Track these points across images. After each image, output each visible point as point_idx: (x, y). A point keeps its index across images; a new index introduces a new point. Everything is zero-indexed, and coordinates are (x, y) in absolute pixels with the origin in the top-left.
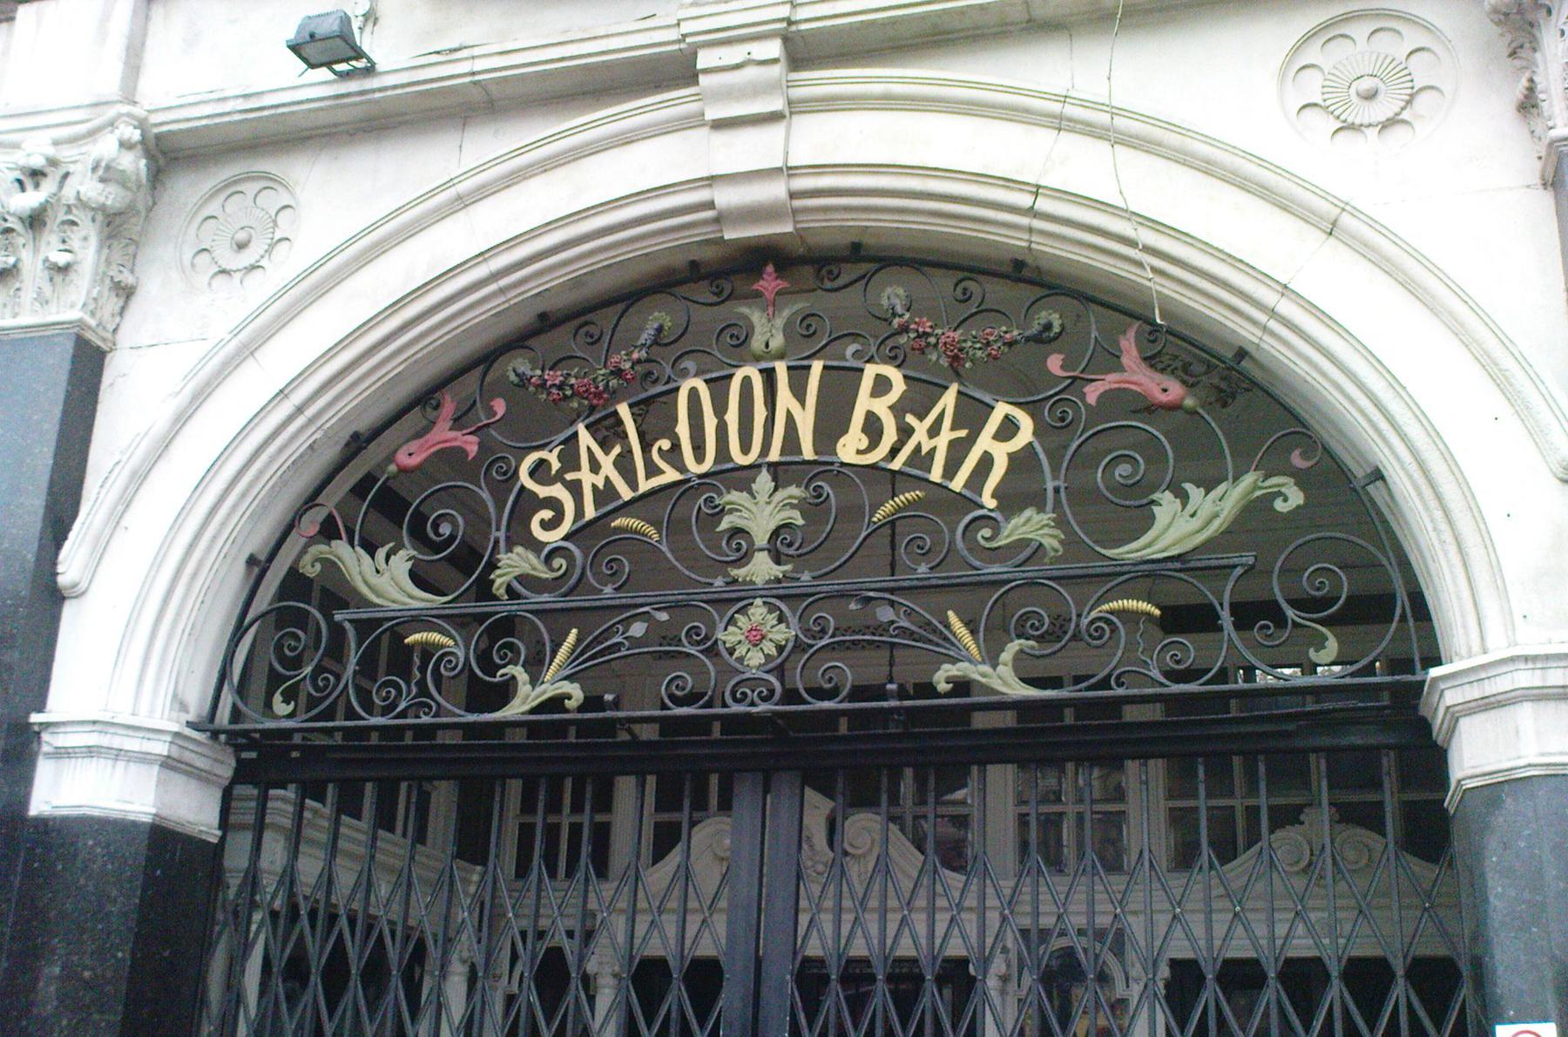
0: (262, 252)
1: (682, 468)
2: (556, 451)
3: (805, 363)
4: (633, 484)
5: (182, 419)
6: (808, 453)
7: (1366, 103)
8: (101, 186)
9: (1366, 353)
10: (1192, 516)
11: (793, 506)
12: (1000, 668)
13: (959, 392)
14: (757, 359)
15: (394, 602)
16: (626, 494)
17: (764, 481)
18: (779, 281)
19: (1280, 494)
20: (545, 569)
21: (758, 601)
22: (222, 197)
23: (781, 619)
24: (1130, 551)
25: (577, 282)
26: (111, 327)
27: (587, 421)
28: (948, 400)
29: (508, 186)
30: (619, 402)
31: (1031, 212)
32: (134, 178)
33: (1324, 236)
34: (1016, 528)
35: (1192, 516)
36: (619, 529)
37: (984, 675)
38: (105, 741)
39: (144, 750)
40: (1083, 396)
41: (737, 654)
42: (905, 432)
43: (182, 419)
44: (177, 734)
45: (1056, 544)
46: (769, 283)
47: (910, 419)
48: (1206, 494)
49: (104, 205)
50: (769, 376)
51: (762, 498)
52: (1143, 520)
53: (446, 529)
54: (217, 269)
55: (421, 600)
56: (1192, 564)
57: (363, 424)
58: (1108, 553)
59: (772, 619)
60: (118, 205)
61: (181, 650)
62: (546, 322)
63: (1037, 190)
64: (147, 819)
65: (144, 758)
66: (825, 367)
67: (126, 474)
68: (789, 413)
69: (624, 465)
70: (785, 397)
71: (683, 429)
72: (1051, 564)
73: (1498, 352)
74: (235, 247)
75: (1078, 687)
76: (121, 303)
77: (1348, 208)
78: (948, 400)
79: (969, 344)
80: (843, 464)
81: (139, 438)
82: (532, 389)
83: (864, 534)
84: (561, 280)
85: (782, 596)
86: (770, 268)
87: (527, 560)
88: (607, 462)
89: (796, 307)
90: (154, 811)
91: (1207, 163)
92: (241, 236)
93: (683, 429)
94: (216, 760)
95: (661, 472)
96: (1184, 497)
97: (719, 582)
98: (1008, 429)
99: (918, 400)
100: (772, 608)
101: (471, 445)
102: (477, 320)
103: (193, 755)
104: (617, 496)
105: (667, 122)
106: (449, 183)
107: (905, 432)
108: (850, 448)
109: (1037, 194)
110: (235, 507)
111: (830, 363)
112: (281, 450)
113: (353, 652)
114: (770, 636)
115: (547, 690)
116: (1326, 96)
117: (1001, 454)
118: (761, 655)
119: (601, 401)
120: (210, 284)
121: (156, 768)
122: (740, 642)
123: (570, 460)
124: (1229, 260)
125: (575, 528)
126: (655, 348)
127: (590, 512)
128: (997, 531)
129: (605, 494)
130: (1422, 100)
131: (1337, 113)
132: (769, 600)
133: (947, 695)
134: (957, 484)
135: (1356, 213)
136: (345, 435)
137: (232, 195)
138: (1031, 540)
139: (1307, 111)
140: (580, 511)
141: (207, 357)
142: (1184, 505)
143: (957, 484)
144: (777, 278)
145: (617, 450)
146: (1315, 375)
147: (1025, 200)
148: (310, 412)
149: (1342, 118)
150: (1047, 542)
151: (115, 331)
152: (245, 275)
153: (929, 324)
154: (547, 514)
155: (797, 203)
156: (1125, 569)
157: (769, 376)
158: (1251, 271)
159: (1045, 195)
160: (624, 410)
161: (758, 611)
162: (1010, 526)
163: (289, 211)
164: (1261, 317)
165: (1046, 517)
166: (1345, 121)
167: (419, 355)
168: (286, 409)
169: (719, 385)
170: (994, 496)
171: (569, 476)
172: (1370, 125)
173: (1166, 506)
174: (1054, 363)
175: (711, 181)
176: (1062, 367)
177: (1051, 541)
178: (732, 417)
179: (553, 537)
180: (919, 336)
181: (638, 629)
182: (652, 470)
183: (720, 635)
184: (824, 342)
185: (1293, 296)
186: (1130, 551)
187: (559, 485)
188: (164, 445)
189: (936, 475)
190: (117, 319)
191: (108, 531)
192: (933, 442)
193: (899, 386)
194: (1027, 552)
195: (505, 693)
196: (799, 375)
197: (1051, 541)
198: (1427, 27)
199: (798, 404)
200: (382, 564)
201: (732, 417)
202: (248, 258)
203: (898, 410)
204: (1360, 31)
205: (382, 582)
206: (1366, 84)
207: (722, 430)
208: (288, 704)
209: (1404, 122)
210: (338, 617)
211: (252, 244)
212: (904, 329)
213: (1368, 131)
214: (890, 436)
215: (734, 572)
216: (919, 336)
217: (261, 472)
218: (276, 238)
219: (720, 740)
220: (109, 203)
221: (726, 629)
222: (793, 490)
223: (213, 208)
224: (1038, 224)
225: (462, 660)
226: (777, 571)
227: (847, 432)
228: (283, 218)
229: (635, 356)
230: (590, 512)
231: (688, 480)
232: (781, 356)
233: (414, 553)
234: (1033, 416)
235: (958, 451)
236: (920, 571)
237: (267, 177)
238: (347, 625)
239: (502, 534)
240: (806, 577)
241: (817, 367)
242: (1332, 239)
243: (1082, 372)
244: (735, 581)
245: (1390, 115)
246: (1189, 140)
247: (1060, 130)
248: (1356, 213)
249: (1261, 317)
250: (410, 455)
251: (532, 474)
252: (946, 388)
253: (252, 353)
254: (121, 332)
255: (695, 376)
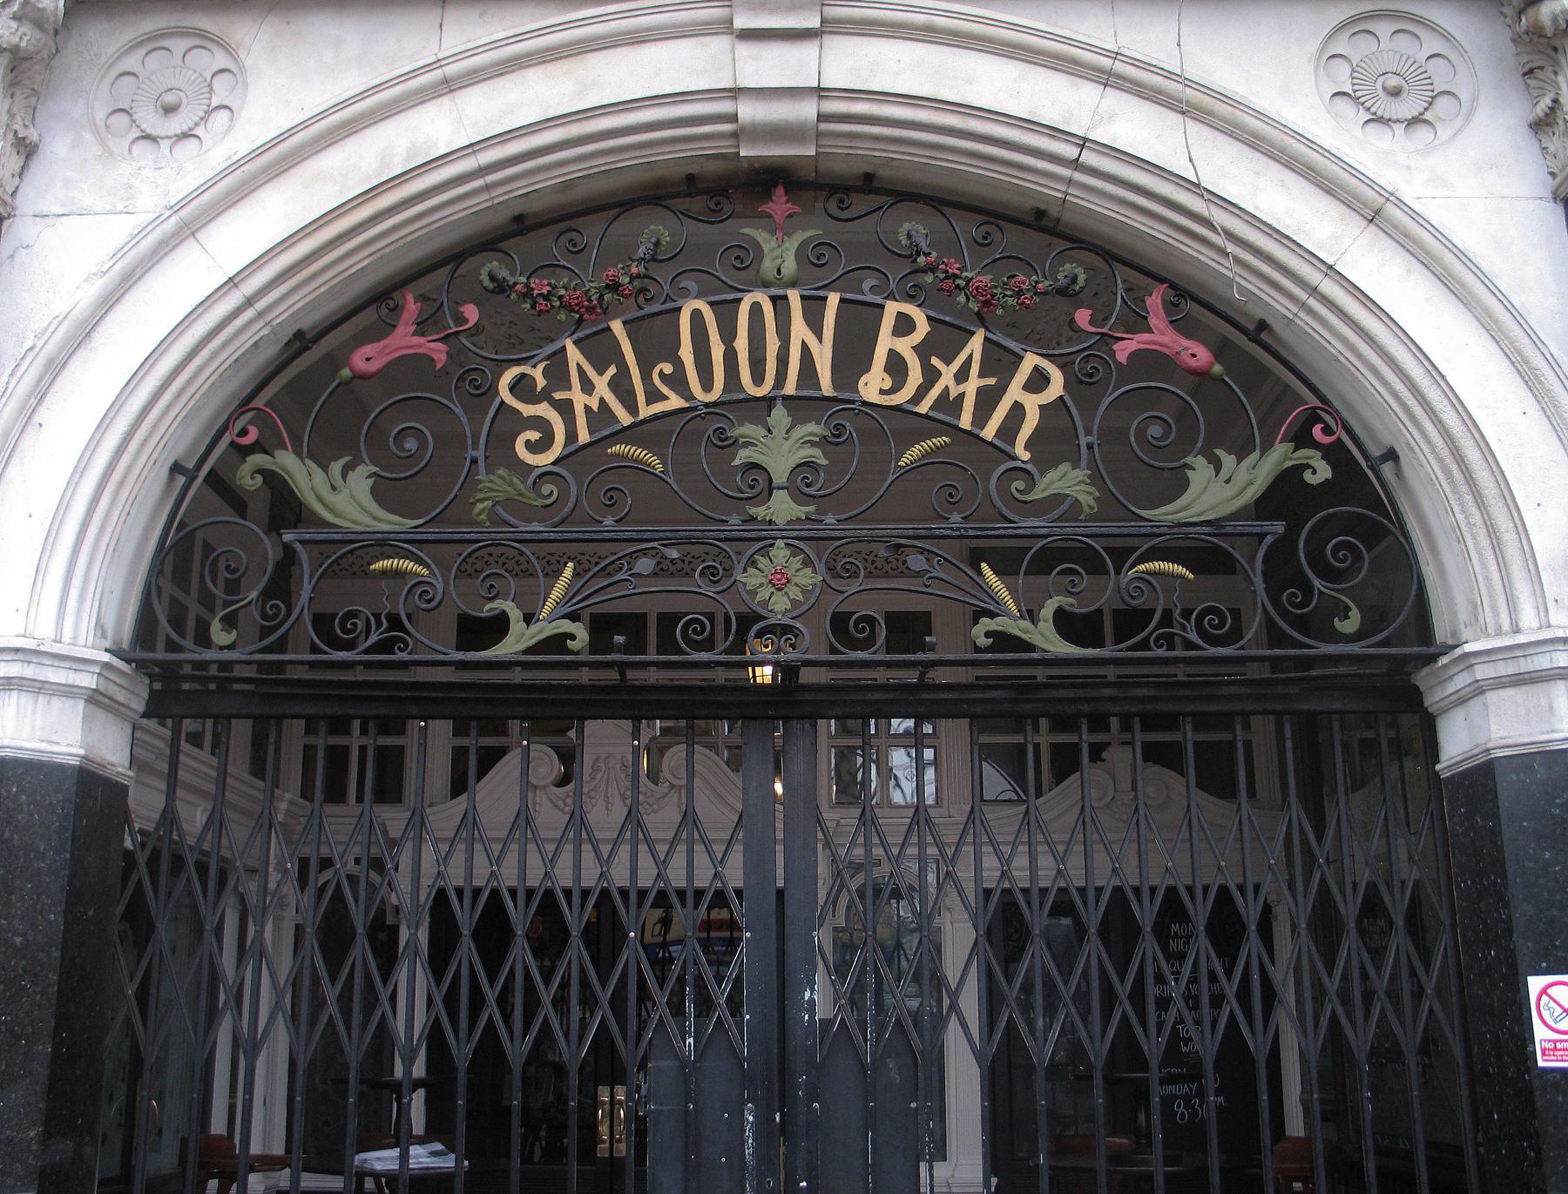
0: (197, 119)
1: (685, 393)
2: (541, 367)
3: (821, 293)
4: (632, 408)
5: (109, 302)
6: (826, 387)
7: (1393, 99)
8: (14, 24)
9: (1406, 340)
10: (1228, 481)
11: (813, 444)
12: (1041, 624)
13: (986, 339)
14: (766, 285)
15: (355, 522)
16: (625, 419)
17: (779, 414)
18: (789, 205)
19: (1308, 466)
20: (533, 495)
21: (780, 543)
22: (142, 52)
23: (808, 562)
24: (1165, 513)
25: (567, 185)
26: (10, 190)
27: (575, 336)
28: (976, 345)
29: (501, 74)
30: (614, 318)
31: (1075, 164)
32: (52, 19)
33: (1365, 223)
34: (1052, 482)
35: (1228, 481)
36: (616, 455)
37: (1026, 632)
38: (29, 671)
39: (70, 682)
40: (1113, 354)
41: (759, 598)
42: (931, 376)
43: (109, 302)
44: (106, 666)
45: (1093, 503)
46: (779, 204)
47: (935, 361)
48: (1239, 461)
49: (17, 47)
50: (779, 302)
51: (779, 432)
52: (1178, 484)
53: (411, 444)
54: (138, 134)
55: (388, 522)
56: (1229, 530)
57: (306, 323)
58: (1144, 513)
59: (796, 562)
60: (31, 48)
61: (104, 569)
62: (521, 224)
63: (1083, 143)
64: (74, 762)
65: (68, 691)
66: (842, 300)
67: (40, 361)
68: (804, 345)
69: (621, 386)
70: (799, 329)
71: (686, 353)
72: (1086, 521)
73: (1530, 352)
74: (161, 110)
75: (1121, 646)
76: (21, 163)
77: (1392, 198)
78: (976, 345)
79: (1000, 290)
80: (865, 403)
81: (56, 322)
82: (513, 296)
83: (891, 478)
84: (553, 182)
85: (805, 539)
86: (780, 191)
87: (511, 484)
88: (601, 384)
89: (809, 233)
90: (82, 752)
91: (1256, 137)
92: (170, 99)
93: (686, 353)
94: (133, 693)
95: (665, 398)
96: (1217, 465)
97: (735, 520)
98: (1038, 382)
99: (942, 342)
100: (795, 550)
101: (439, 353)
102: (455, 217)
103: (116, 688)
104: (616, 420)
105: (686, 25)
106: (437, 63)
107: (931, 376)
108: (873, 385)
109: (1082, 147)
110: (169, 407)
111: (849, 296)
112: (224, 345)
113: (306, 579)
114: (795, 580)
115: (544, 629)
116: (1356, 87)
117: (1033, 404)
118: (786, 599)
119: (593, 317)
120: (130, 150)
121: (81, 704)
122: (762, 585)
123: (558, 372)
124: (1276, 236)
125: (567, 451)
126: (652, 265)
127: (584, 436)
128: (1032, 482)
129: (601, 415)
130: (1443, 103)
131: (1367, 105)
132: (790, 541)
133: (987, 650)
134: (989, 432)
135: (1400, 204)
136: (293, 330)
137: (150, 52)
138: (1067, 495)
139: (1338, 100)
140: (571, 435)
141: (137, 237)
142: (1218, 470)
143: (989, 432)
144: (787, 202)
145: (612, 371)
146: (1348, 355)
147: (1070, 151)
148: (260, 305)
149: (1373, 110)
150: (1083, 498)
151: (14, 194)
152: (174, 143)
153: (957, 266)
154: (533, 435)
155: (824, 126)
156: (1162, 530)
157: (779, 302)
158: (1296, 249)
159: (1089, 148)
160: (617, 327)
161: (780, 552)
162: (1046, 480)
163: (226, 76)
164: (1302, 295)
165: (1081, 474)
166: (1375, 114)
167: (387, 250)
168: (234, 299)
169: (726, 312)
170: (1026, 448)
171: (558, 396)
172: (1398, 121)
173: (1200, 472)
174: (1083, 317)
175: (736, 93)
176: (1091, 323)
177: (1086, 497)
178: (742, 344)
179: (544, 460)
180: (947, 278)
181: (645, 565)
182: (654, 396)
183: (740, 577)
184: (838, 274)
185: (1337, 278)
186: (1165, 513)
187: (545, 405)
188: (84, 332)
189: (966, 421)
190: (17, 180)
191: (18, 428)
192: (961, 388)
193: (923, 328)
194: (1065, 506)
195: (498, 627)
196: (815, 307)
197: (1086, 497)
198: (1446, 36)
199: (817, 341)
200: (338, 481)
201: (742, 344)
202: (177, 124)
203: (922, 350)
204: (1384, 29)
205: (340, 500)
206: (1393, 81)
207: (731, 357)
208: (229, 633)
209: (1426, 122)
210: (288, 537)
211: (181, 109)
212: (931, 268)
213: (1396, 127)
214: (915, 377)
215: (753, 511)
216: (947, 278)
217: (201, 369)
218: (213, 105)
219: (1184, 682)
220: (24, 44)
221: (745, 570)
222: (812, 427)
223: (131, 63)
224: (1079, 177)
225: (440, 591)
226: (801, 511)
227: (869, 370)
228: (221, 83)
229: (634, 270)
230: (584, 436)
231: (695, 409)
232: (793, 284)
233: (374, 469)
234: (1062, 367)
235: (987, 400)
236: (952, 520)
237: (201, 34)
238: (298, 547)
239: (480, 454)
240: (830, 519)
241: (834, 299)
242: (1372, 227)
243: (1110, 330)
244: (753, 519)
245: (1415, 114)
246: (1241, 113)
247: (1106, 85)
248: (1400, 203)
249: (1302, 295)
250: (368, 359)
251: (512, 388)
252: (973, 333)
253: (193, 234)
254: (19, 195)
255: (696, 297)
